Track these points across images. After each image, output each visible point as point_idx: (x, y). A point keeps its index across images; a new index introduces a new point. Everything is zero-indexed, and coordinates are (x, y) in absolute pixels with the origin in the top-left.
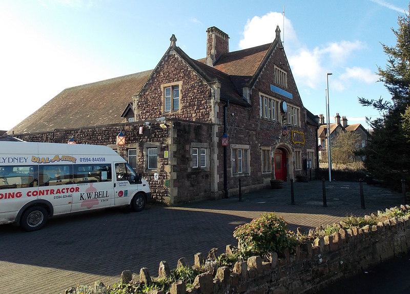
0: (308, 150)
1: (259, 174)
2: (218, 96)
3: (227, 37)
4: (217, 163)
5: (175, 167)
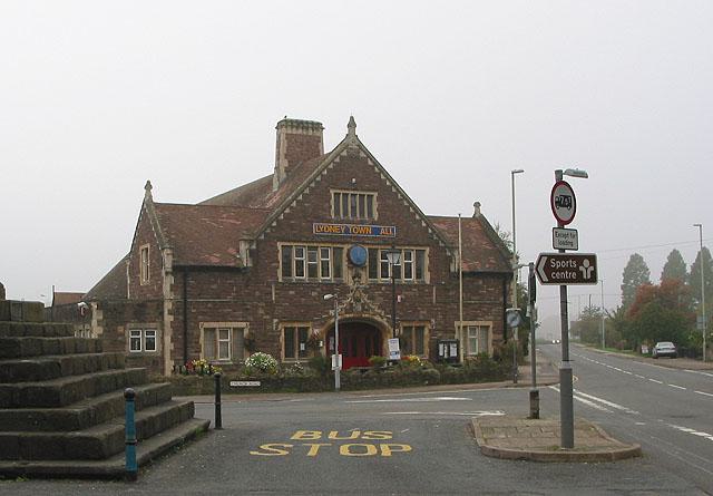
4: (169, 346)
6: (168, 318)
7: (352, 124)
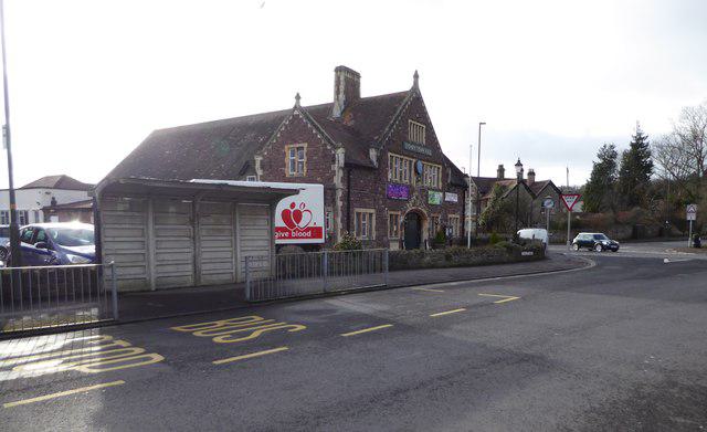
0: (450, 216)
1: (385, 239)
2: (342, 162)
3: (357, 75)
4: (340, 226)
5: (522, 186)
6: (340, 204)
7: (416, 76)
